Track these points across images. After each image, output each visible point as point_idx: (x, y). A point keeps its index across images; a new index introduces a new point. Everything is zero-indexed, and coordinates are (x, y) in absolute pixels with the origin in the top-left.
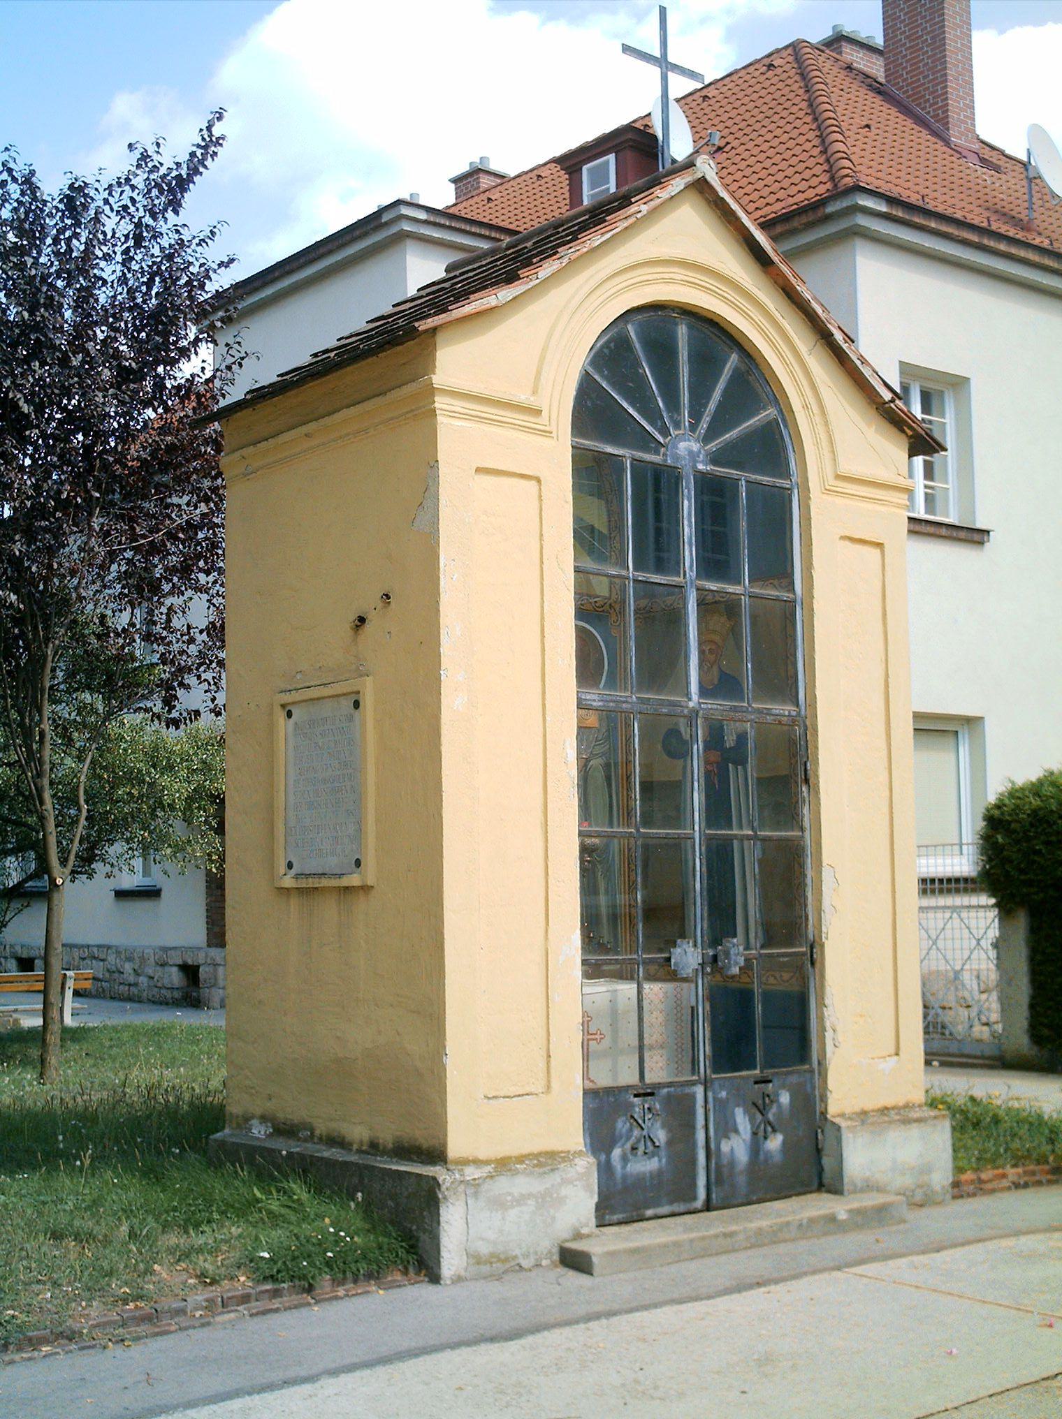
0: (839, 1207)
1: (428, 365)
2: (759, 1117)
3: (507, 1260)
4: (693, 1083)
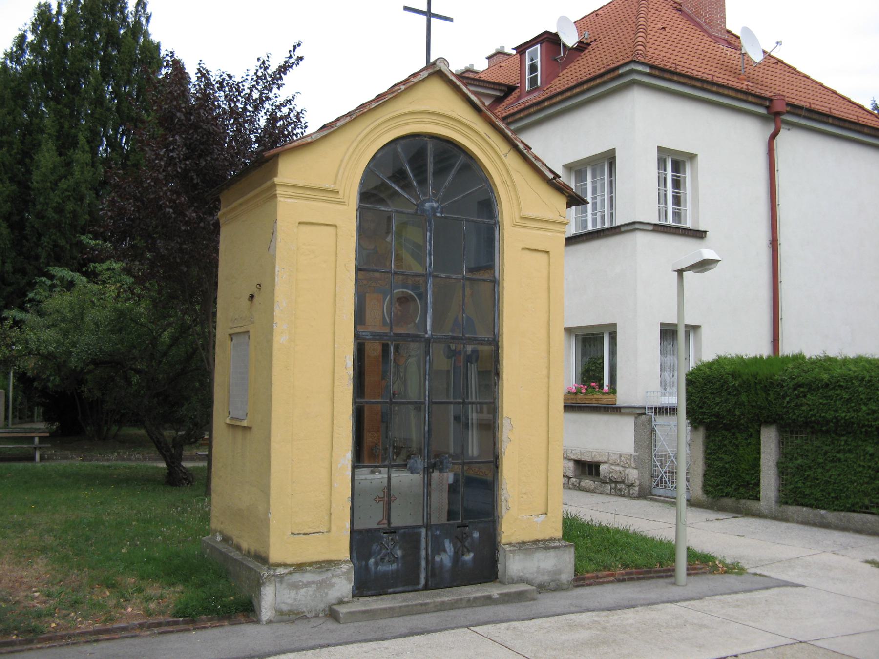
0: (494, 591)
1: (274, 172)
2: (459, 544)
3: (298, 613)
4: (420, 527)
